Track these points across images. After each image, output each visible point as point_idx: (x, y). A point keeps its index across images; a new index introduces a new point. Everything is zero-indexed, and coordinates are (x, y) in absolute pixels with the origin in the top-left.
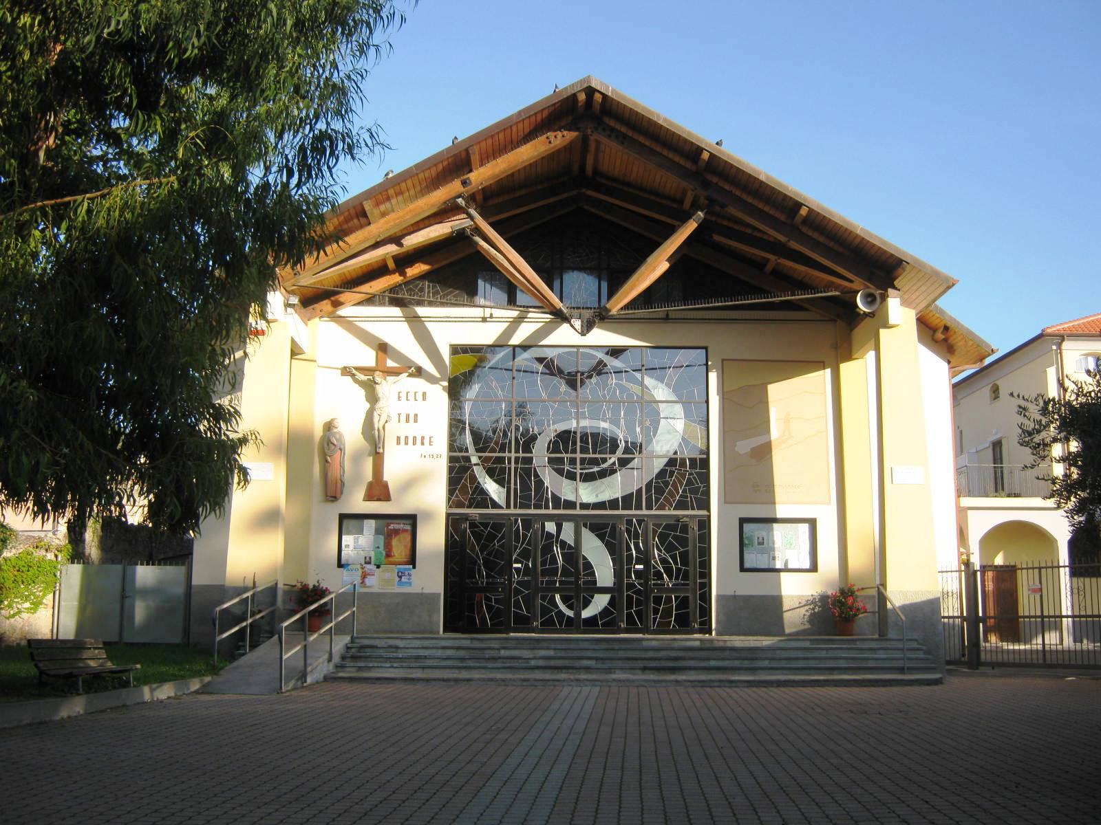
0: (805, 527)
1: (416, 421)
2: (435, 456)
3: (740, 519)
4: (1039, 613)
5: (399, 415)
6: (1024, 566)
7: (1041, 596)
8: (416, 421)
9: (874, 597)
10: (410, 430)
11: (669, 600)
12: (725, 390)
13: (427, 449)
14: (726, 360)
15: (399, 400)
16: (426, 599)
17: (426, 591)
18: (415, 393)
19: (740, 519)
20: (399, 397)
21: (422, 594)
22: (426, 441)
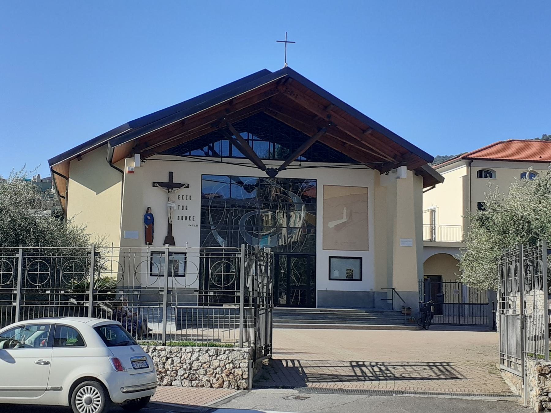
0: (331, 259)
1: (187, 209)
2: (195, 225)
3: (362, 258)
4: (457, 302)
5: (179, 206)
6: (452, 281)
7: (459, 295)
8: (187, 209)
9: (353, 278)
10: (185, 213)
11: (297, 292)
12: (324, 199)
13: (192, 222)
14: (325, 185)
15: (179, 199)
16: (190, 291)
17: (462, 214)
18: (183, 196)
19: (362, 258)
20: (179, 198)
21: (422, 224)
22: (191, 218)
